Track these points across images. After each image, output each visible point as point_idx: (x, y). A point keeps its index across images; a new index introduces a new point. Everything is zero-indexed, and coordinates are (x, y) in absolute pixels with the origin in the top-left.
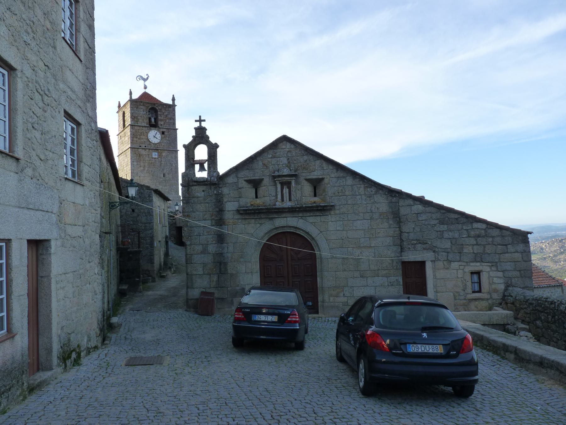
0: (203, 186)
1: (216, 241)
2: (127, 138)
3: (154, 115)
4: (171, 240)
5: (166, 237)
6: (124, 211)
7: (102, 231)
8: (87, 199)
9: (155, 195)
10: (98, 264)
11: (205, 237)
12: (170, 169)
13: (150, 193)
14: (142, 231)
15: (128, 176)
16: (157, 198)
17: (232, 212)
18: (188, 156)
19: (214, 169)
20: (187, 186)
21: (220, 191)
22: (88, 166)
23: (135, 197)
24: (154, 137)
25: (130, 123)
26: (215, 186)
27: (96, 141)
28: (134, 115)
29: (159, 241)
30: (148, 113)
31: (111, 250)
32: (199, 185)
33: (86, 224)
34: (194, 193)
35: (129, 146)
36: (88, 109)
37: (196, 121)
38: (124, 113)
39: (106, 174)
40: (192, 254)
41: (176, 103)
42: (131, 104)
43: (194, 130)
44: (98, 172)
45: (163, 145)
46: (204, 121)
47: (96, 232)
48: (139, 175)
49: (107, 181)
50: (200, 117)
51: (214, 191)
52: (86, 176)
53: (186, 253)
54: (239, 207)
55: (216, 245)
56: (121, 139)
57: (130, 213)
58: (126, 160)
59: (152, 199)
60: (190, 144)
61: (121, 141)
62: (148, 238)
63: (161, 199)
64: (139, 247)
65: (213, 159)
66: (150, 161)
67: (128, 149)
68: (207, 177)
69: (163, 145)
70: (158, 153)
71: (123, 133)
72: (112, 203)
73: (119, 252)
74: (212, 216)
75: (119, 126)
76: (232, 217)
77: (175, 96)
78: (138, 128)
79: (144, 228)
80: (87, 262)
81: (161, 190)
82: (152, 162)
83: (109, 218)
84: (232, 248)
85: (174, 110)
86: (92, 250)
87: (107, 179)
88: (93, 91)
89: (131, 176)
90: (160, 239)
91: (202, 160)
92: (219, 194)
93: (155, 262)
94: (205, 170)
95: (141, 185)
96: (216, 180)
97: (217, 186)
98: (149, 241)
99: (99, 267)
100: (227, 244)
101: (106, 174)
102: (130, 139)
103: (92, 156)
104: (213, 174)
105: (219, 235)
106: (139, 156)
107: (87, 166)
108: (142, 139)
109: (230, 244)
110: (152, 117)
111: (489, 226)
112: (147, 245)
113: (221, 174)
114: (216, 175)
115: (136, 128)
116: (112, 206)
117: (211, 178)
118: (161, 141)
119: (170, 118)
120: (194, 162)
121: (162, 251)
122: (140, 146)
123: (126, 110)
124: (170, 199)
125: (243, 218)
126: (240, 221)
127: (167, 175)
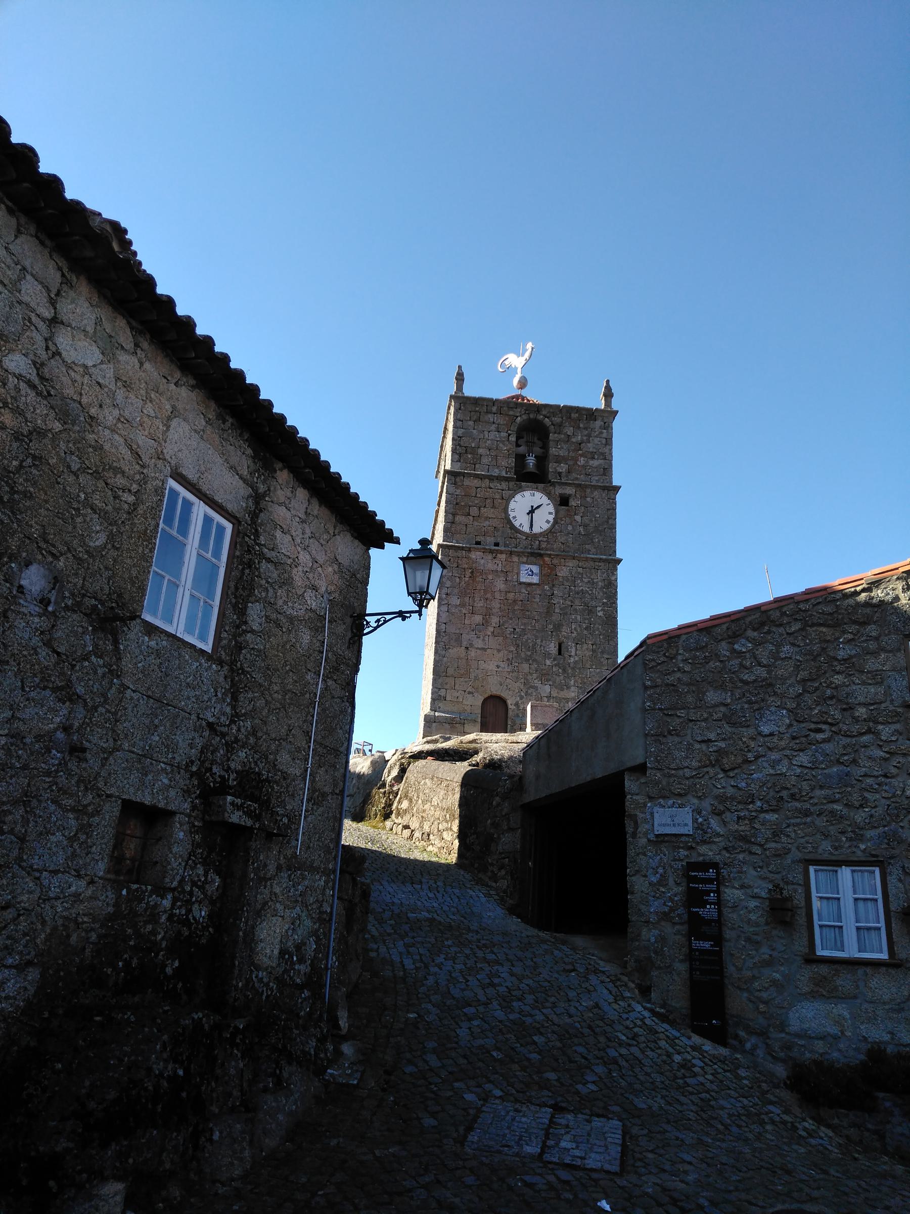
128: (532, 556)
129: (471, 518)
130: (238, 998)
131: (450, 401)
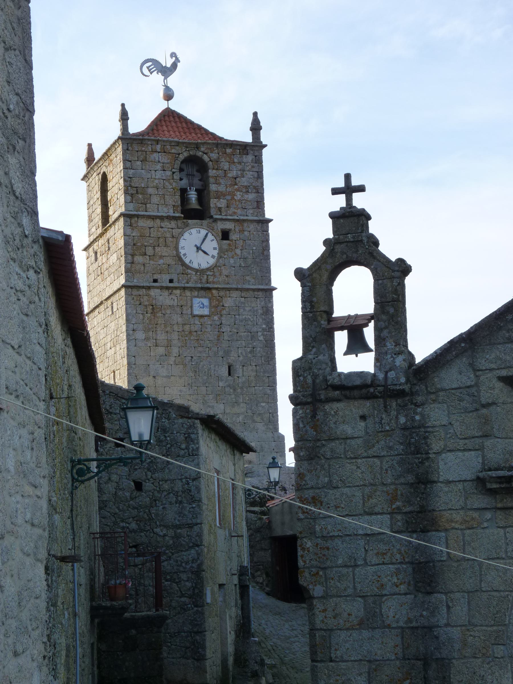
0: (361, 402)
1: (409, 584)
2: (114, 258)
3: (196, 181)
4: (257, 583)
5: (242, 572)
6: (110, 488)
7: (52, 552)
8: (12, 453)
9: (206, 433)
10: (40, 659)
11: (371, 569)
12: (249, 350)
13: (190, 427)
14: (165, 553)
15: (117, 376)
16: (212, 445)
17: (460, 486)
18: (312, 307)
19: (397, 344)
20: (307, 403)
21: (417, 418)
22: (13, 347)
23: (149, 441)
24: (198, 248)
25: (123, 210)
26: (399, 401)
27: (36, 272)
28: (136, 183)
29: (221, 586)
30: (177, 176)
31: (75, 615)
32: (348, 398)
33: (8, 532)
34: (332, 425)
35: (122, 280)
36: (12, 174)
37: (335, 191)
38: (104, 180)
39: (61, 373)
40: (332, 630)
41: (264, 139)
42: (125, 151)
43: (330, 221)
44: (43, 367)
45: (225, 272)
46: (361, 189)
47: (35, 554)
48: (152, 373)
49: (65, 395)
50: (348, 177)
51: (397, 417)
52: (7, 379)
53: (312, 623)
54: (484, 470)
55: (410, 597)
56: (96, 259)
57: (128, 494)
58: (113, 326)
59: (198, 448)
60: (317, 265)
61: (95, 265)
62: (184, 576)
63: (223, 447)
64: (158, 604)
65: (392, 310)
66: (187, 328)
67: (119, 290)
68: (372, 371)
69: (225, 272)
70: (210, 299)
71: (101, 241)
72: (80, 462)
73: (96, 621)
74: (394, 499)
75: (90, 220)
76: (461, 503)
77: (259, 116)
78: (149, 223)
79: (171, 542)
80: (10, 654)
81: (220, 416)
82: (193, 328)
83: (72, 511)
84: (465, 609)
85: (258, 161)
86: (25, 615)
87: (66, 388)
88: (26, 118)
89: (129, 374)
90: (222, 580)
91: (357, 316)
92: (413, 428)
93: (209, 653)
94: (366, 349)
95: (163, 404)
96: (403, 380)
97: (407, 398)
98: (188, 584)
99: (45, 669)
100: (446, 594)
101: (61, 373)
102: (123, 259)
103: (25, 318)
104: (394, 362)
105: (420, 563)
106: (153, 312)
107: (11, 350)
108: (161, 257)
109: (458, 595)
110: (191, 185)
111: (100, 462)
112: (183, 599)
113: (419, 359)
114: (405, 365)
115: (142, 223)
116: (80, 473)
117: (386, 373)
118: (218, 261)
119: (246, 187)
120: (333, 325)
121: (231, 617)
122: (155, 281)
123: (110, 168)
124: (253, 444)
125: (499, 505)
126: (488, 515)
127: (239, 370)
129: (148, 257)
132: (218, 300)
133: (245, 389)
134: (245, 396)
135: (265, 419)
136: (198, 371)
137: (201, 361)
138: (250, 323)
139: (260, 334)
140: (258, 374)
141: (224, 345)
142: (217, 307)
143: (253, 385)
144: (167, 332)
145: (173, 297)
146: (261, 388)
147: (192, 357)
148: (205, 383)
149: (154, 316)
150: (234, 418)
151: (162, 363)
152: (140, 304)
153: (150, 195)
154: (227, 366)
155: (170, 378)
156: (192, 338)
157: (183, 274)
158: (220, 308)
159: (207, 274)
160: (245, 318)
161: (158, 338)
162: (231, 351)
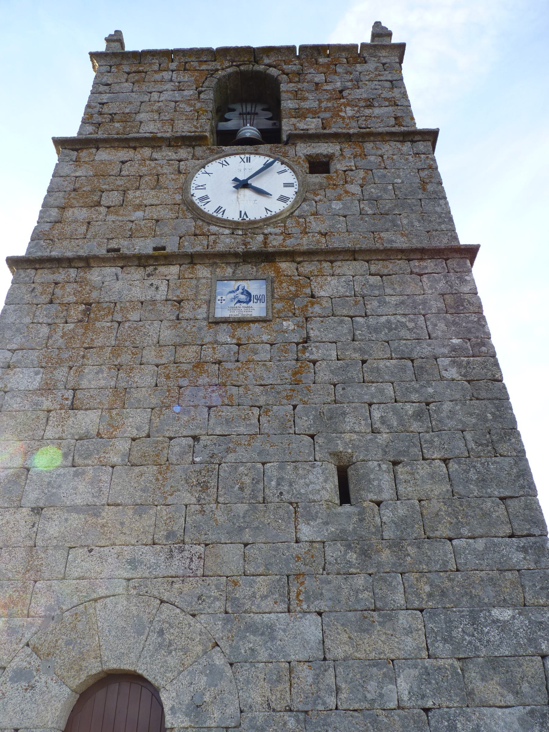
12: (410, 409)
128: (245, 262)
129: (103, 210)
130: (68, 673)
131: (92, 60)
132: (296, 283)
133: (411, 550)
134: (412, 577)
135: (525, 687)
136: (213, 483)
137: (228, 450)
138: (403, 333)
139: (444, 362)
140: (459, 489)
141: (316, 399)
142: (292, 299)
143: (443, 531)
144: (119, 367)
145: (155, 282)
146: (480, 544)
147: (196, 438)
148: (241, 529)
149: (86, 329)
150: (372, 686)
151: (78, 461)
152: (51, 302)
153: (141, 122)
154: (332, 469)
155: (97, 515)
156: (200, 382)
157: (195, 235)
158: (298, 303)
159: (266, 231)
160: (389, 321)
161: (84, 384)
162: (344, 414)
